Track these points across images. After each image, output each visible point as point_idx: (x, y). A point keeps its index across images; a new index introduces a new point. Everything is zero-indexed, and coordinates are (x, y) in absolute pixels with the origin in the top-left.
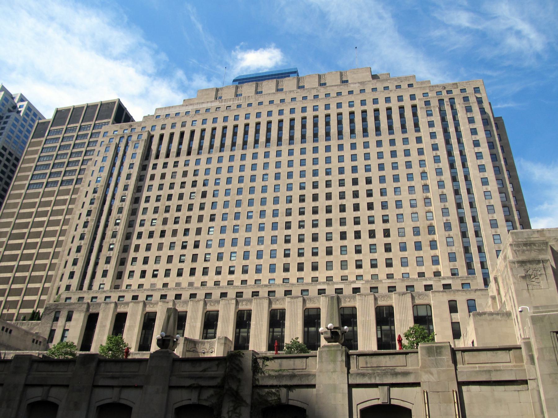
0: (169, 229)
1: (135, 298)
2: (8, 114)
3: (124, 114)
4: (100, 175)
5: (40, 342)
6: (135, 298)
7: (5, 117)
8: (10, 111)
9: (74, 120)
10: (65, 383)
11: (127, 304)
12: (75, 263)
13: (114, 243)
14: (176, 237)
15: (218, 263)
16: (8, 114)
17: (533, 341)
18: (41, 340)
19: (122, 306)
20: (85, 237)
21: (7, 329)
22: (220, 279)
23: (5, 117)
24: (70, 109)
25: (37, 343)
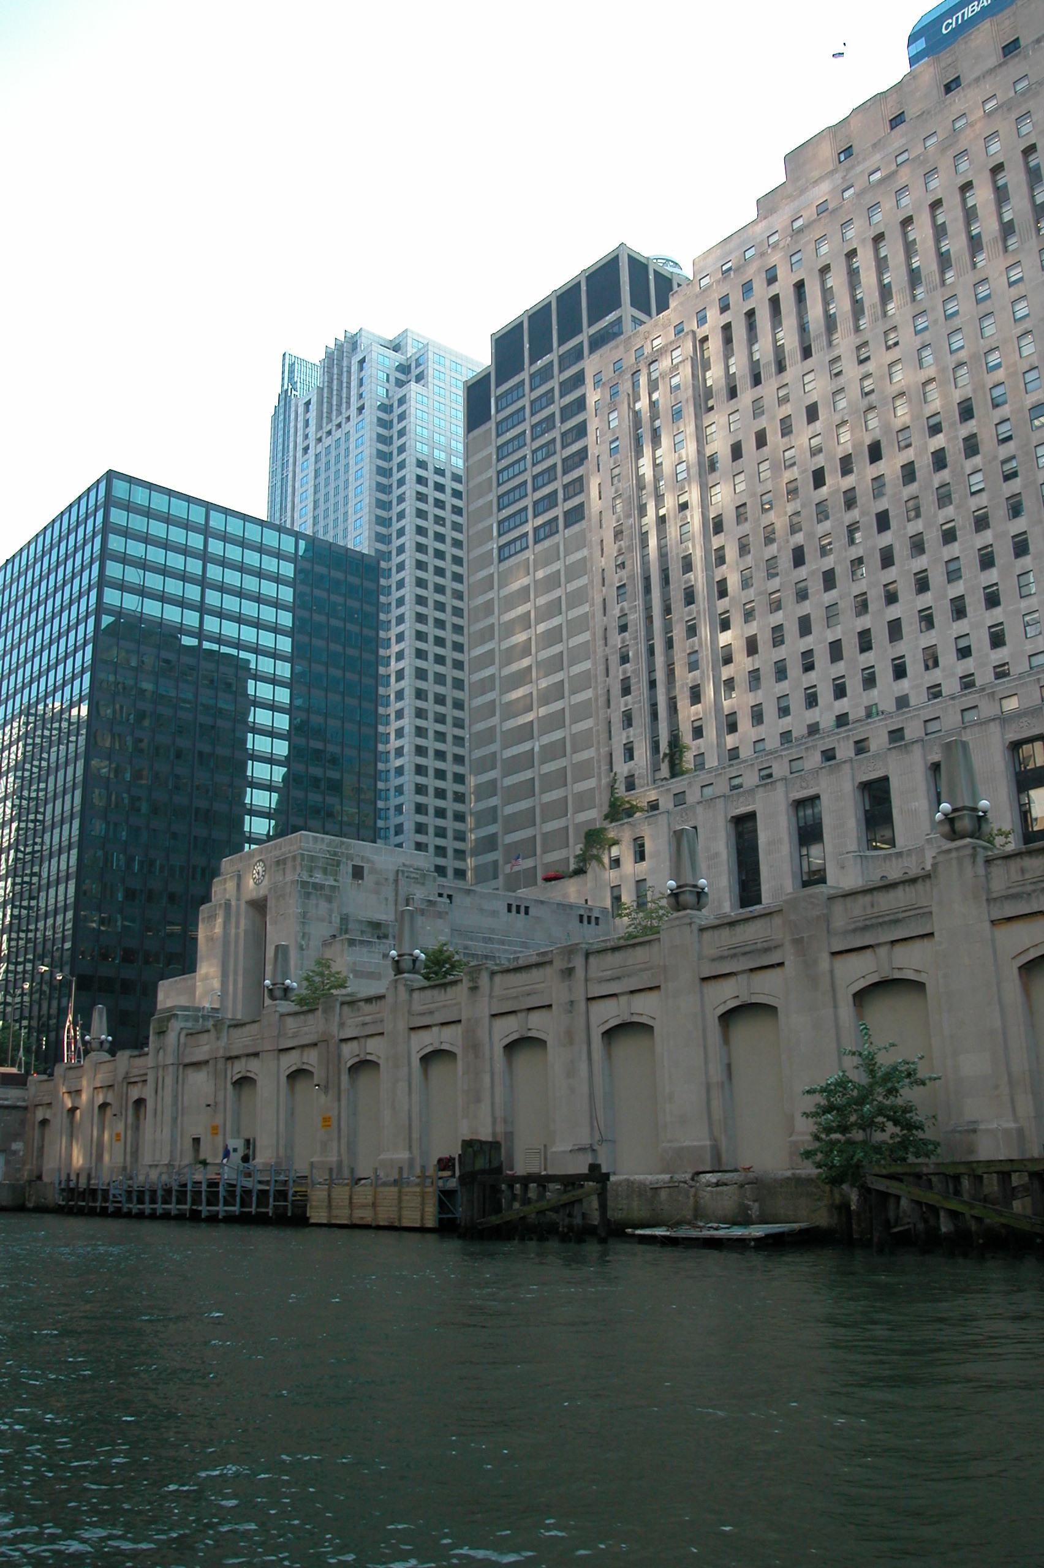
0: (813, 573)
1: (896, 735)
2: (400, 392)
3: (651, 277)
4: (680, 458)
5: (597, 918)
6: (896, 735)
7: (396, 405)
8: (400, 384)
9: (541, 348)
10: (840, 958)
11: (752, 791)
12: (628, 720)
13: (696, 648)
14: (893, 568)
15: (955, 625)
16: (400, 392)
17: (343, 991)
18: (595, 914)
19: (741, 799)
20: (631, 654)
21: (518, 907)
22: (972, 668)
23: (396, 405)
24: (522, 323)
25: (589, 922)
